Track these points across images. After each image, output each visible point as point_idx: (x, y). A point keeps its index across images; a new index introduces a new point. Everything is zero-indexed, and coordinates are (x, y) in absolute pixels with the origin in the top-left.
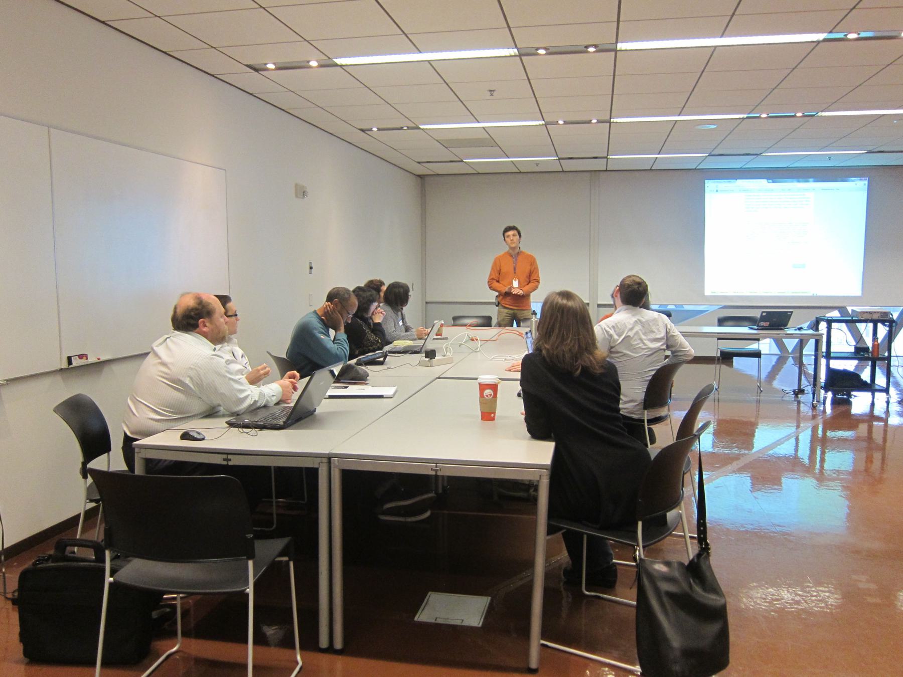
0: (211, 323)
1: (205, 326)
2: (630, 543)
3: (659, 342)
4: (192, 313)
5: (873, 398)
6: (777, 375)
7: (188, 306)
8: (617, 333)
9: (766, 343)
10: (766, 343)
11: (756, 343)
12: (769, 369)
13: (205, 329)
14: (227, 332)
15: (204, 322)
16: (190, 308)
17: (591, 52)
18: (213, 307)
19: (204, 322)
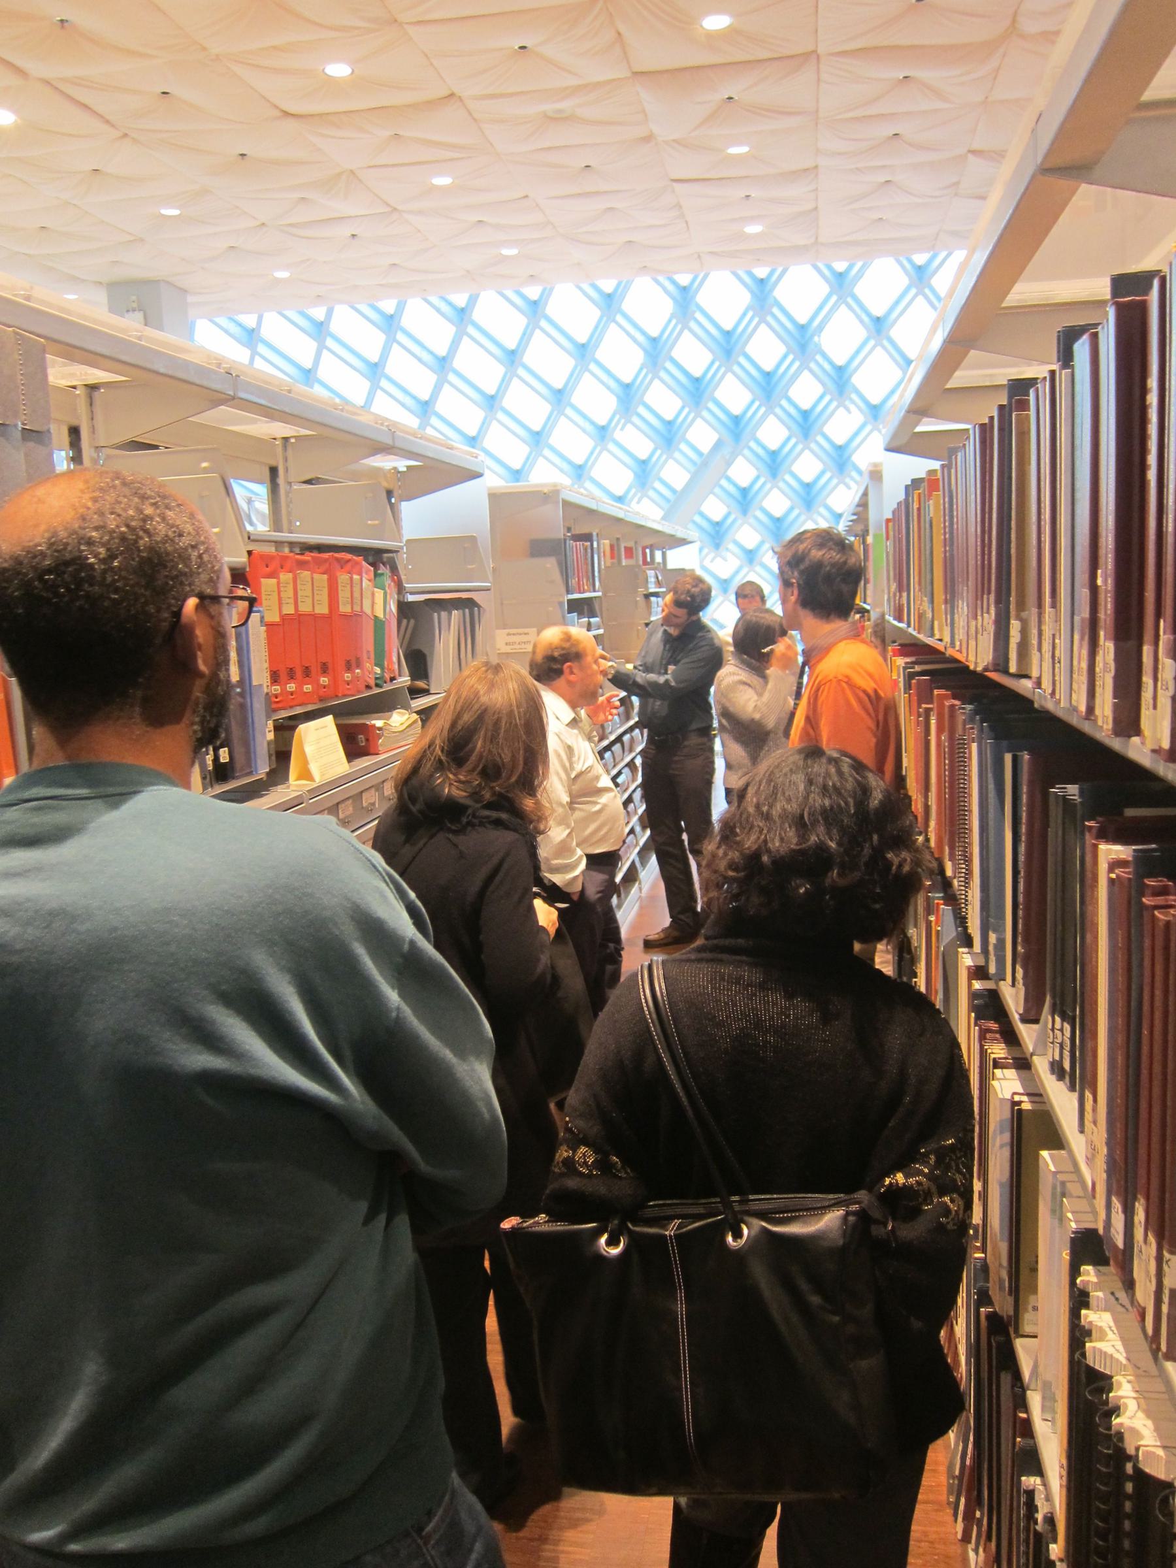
0: (581, 669)
1: (572, 673)
2: (1014, 463)
3: (1104, 1228)
4: (556, 654)
5: (630, 67)
6: (1116, 1410)
7: (551, 644)
8: (610, 677)
9: (313, 607)
10: (313, 607)
11: (715, 621)
12: (1113, 1205)
13: (572, 677)
14: (379, 723)
15: (570, 667)
16: (554, 646)
17: (840, 641)
18: (757, 622)
19: (570, 667)
